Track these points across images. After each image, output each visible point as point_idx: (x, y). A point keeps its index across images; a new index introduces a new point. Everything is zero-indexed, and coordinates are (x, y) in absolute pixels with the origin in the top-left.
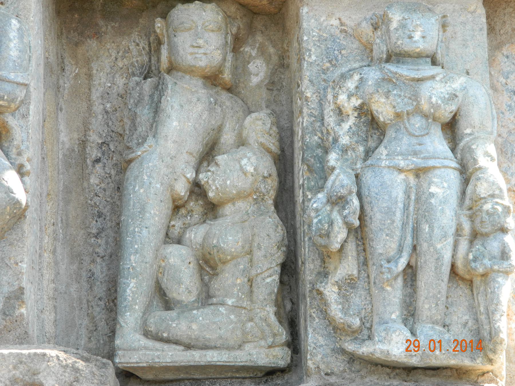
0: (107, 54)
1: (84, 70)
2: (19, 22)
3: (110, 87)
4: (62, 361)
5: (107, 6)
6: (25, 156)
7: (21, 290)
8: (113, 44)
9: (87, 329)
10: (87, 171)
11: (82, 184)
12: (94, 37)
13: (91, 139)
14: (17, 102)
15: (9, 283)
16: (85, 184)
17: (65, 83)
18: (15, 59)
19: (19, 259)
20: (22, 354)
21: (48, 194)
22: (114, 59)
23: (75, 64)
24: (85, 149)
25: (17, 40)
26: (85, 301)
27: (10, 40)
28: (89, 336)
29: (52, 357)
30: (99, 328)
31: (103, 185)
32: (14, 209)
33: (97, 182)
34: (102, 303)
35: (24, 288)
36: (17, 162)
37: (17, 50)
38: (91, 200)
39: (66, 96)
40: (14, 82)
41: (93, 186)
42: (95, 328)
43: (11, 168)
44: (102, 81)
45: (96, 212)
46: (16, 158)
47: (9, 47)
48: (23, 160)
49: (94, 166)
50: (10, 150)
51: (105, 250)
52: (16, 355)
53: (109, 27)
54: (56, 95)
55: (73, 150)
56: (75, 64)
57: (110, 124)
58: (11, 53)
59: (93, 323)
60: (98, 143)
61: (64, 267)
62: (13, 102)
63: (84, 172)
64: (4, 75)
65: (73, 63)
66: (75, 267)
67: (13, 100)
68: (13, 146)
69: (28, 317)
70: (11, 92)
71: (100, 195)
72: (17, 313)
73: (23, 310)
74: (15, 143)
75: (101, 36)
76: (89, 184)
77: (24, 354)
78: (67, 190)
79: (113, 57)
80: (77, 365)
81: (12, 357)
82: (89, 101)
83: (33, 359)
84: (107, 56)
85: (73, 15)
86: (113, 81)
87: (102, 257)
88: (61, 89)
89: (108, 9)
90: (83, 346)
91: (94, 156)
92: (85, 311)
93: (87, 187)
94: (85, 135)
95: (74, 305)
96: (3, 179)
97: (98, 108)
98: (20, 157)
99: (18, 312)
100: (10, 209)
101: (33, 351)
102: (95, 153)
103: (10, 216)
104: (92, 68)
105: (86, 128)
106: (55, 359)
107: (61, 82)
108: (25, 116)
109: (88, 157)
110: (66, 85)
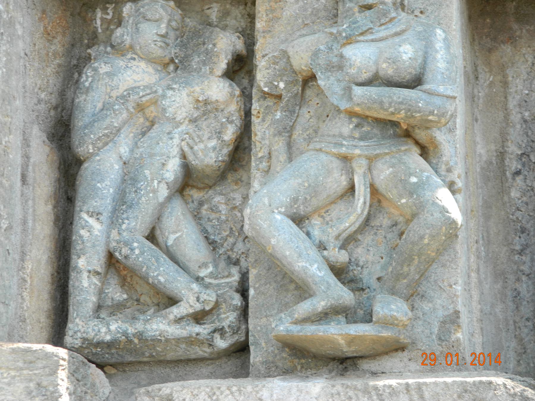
0: (522, 59)
1: (499, 78)
2: (444, 31)
3: (527, 94)
4: (510, 390)
5: (520, 9)
6: (456, 173)
7: (457, 313)
8: (529, 49)
9: (516, 352)
10: (507, 185)
11: (502, 199)
12: (508, 41)
13: (510, 150)
14: (448, 117)
15: (443, 307)
16: (506, 198)
17: (479, 92)
18: (443, 71)
19: (452, 281)
20: (466, 382)
21: (472, 211)
22: (531, 64)
23: (489, 72)
24: (504, 161)
25: (444, 51)
26: (511, 322)
27: (437, 51)
28: (517, 359)
29: (499, 385)
30: (529, 351)
31: (524, 199)
32: (450, 230)
33: (518, 195)
34: (530, 324)
35: (459, 312)
36: (448, 179)
37: (444, 61)
38: (513, 215)
39: (481, 105)
40: (443, 96)
41: (514, 199)
42: (524, 351)
43: (444, 186)
44: (518, 88)
45: (519, 228)
46: (446, 175)
47: (436, 59)
48: (454, 176)
49: (514, 179)
50: (439, 166)
51: (530, 267)
52: (460, 383)
53: (524, 31)
54: (472, 105)
55: (491, 163)
56: (489, 72)
57: (530, 133)
58: (439, 65)
59: (522, 345)
60: (518, 155)
61: (487, 286)
62: (443, 117)
63: (504, 185)
64: (433, 88)
65: (487, 70)
66: (499, 286)
67: (443, 115)
68: (442, 162)
69: (464, 342)
70: (441, 106)
71: (522, 209)
72: (453, 338)
73: (459, 335)
74: (444, 159)
75: (516, 40)
76: (510, 198)
77: (469, 383)
78: (487, 205)
79: (529, 63)
80: (526, 393)
81: (455, 385)
82: (506, 110)
83: (478, 388)
84: (523, 62)
85: (485, 20)
86: (531, 87)
87: (528, 275)
88: (476, 99)
89: (522, 12)
90: (512, 370)
91: (513, 168)
92: (512, 333)
93: (508, 201)
94: (503, 147)
95: (501, 326)
96: (437, 198)
97: (516, 117)
98: (450, 174)
99: (454, 336)
100: (446, 229)
101: (478, 379)
102: (515, 165)
103: (445, 237)
104: (507, 75)
105: (504, 138)
106: (502, 388)
107: (476, 91)
108: (451, 131)
109: (508, 169)
110: (480, 94)
